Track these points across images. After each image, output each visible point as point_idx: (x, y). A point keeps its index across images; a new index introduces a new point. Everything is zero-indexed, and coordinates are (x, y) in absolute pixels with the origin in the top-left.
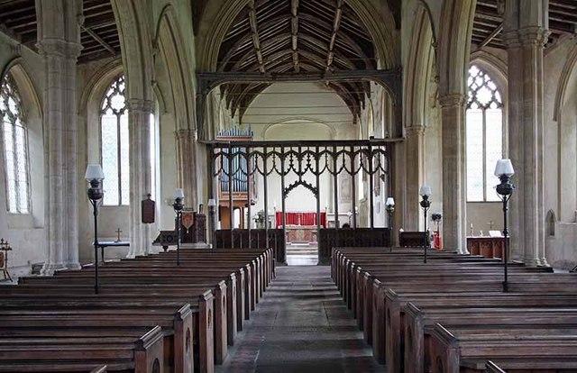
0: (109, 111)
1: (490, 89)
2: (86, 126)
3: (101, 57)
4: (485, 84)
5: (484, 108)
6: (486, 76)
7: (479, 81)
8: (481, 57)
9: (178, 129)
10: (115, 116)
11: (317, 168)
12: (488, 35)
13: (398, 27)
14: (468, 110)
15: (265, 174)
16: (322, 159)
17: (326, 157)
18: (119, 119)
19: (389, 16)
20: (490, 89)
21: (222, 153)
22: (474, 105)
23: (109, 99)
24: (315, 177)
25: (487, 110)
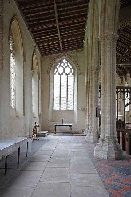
0: (57, 74)
2: (50, 78)
3: (57, 53)
4: (68, 66)
5: (67, 75)
6: (69, 63)
7: (66, 65)
10: (59, 75)
15: (117, 99)
22: (57, 74)
24: (123, 101)
25: (62, 75)
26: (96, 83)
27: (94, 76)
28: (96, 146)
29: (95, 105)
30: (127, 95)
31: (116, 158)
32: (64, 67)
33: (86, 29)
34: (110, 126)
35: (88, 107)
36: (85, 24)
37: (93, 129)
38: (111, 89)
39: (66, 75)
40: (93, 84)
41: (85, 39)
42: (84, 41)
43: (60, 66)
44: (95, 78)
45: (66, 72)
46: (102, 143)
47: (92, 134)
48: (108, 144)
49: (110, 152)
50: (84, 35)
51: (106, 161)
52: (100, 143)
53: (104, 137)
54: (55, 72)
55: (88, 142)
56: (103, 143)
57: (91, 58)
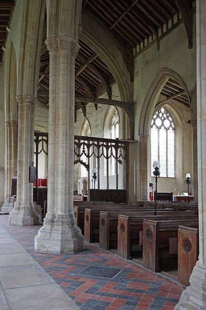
1: (169, 120)
4: (167, 117)
5: (167, 129)
8: (169, 104)
9: (12, 119)
11: (89, 153)
12: (177, 93)
13: (132, 80)
14: (152, 129)
15: (37, 153)
16: (91, 148)
17: (43, 143)
18: (167, 132)
19: (127, 74)
20: (169, 120)
21: (103, 145)
22: (154, 126)
23: (155, 120)
25: (168, 131)
26: (29, 124)
27: (25, 112)
28: (39, 232)
29: (27, 161)
30: (84, 148)
31: (74, 250)
32: (163, 118)
33: (9, 28)
34: (64, 197)
35: (10, 165)
36: (8, 18)
37: (23, 202)
38: (66, 136)
39: (157, 130)
40: (24, 125)
41: (8, 44)
42: (4, 49)
43: (158, 116)
44: (27, 116)
45: (156, 124)
46: (50, 226)
47: (22, 212)
48: (61, 227)
49: (66, 240)
50: (5, 38)
51: (58, 258)
52: (46, 226)
53: (54, 216)
54: (152, 124)
55: (15, 225)
56: (53, 226)
57: (20, 79)
